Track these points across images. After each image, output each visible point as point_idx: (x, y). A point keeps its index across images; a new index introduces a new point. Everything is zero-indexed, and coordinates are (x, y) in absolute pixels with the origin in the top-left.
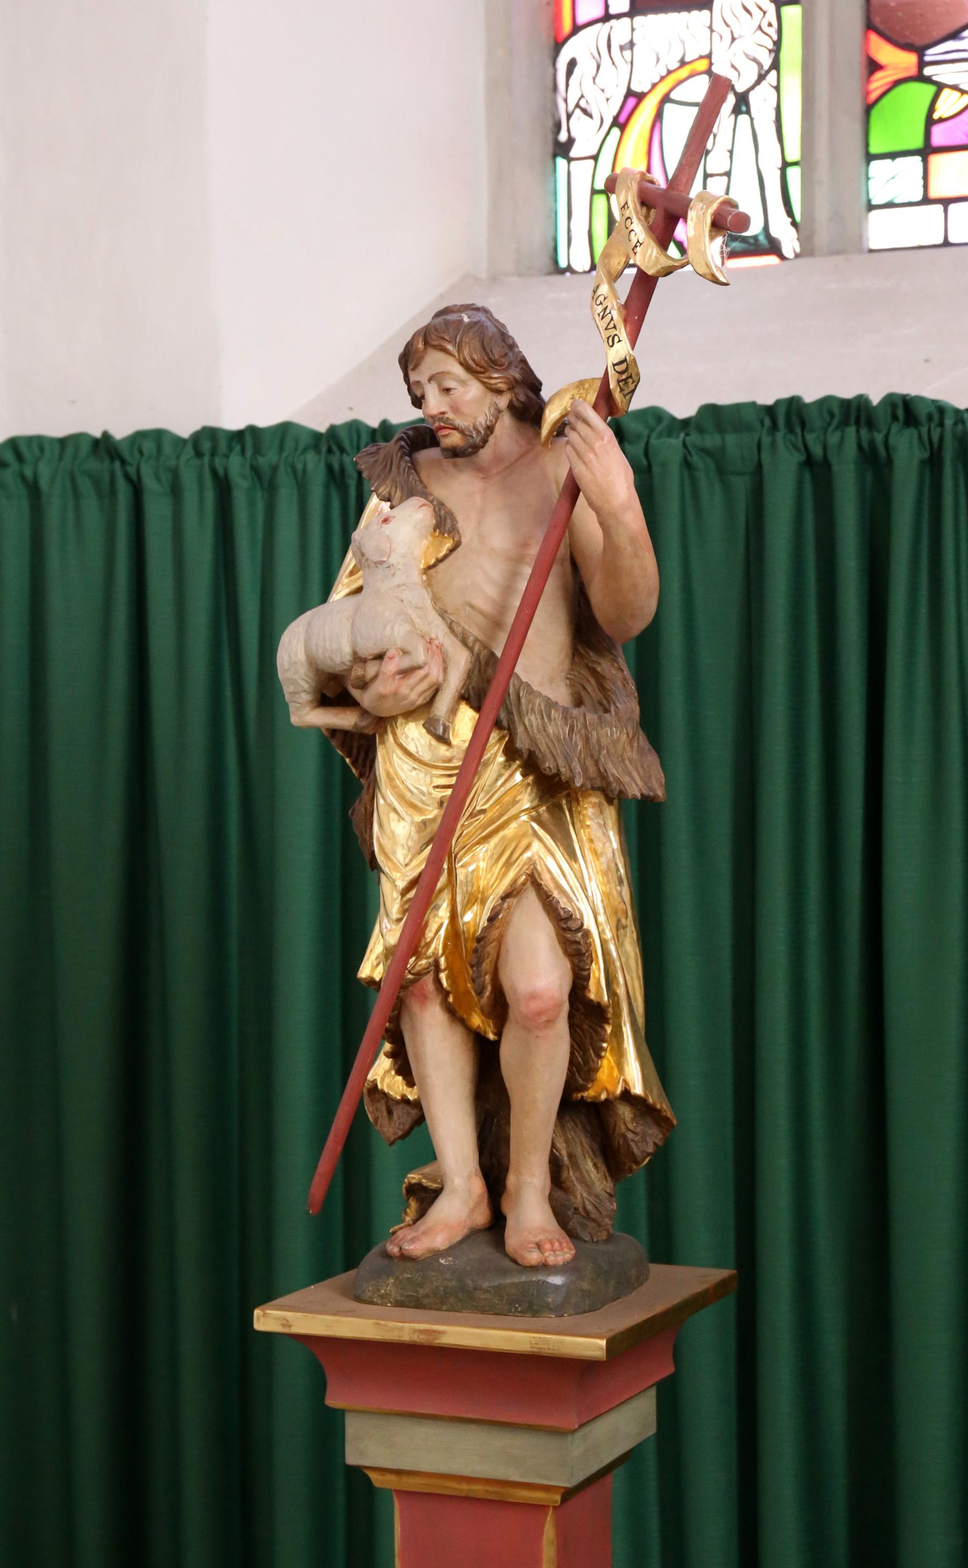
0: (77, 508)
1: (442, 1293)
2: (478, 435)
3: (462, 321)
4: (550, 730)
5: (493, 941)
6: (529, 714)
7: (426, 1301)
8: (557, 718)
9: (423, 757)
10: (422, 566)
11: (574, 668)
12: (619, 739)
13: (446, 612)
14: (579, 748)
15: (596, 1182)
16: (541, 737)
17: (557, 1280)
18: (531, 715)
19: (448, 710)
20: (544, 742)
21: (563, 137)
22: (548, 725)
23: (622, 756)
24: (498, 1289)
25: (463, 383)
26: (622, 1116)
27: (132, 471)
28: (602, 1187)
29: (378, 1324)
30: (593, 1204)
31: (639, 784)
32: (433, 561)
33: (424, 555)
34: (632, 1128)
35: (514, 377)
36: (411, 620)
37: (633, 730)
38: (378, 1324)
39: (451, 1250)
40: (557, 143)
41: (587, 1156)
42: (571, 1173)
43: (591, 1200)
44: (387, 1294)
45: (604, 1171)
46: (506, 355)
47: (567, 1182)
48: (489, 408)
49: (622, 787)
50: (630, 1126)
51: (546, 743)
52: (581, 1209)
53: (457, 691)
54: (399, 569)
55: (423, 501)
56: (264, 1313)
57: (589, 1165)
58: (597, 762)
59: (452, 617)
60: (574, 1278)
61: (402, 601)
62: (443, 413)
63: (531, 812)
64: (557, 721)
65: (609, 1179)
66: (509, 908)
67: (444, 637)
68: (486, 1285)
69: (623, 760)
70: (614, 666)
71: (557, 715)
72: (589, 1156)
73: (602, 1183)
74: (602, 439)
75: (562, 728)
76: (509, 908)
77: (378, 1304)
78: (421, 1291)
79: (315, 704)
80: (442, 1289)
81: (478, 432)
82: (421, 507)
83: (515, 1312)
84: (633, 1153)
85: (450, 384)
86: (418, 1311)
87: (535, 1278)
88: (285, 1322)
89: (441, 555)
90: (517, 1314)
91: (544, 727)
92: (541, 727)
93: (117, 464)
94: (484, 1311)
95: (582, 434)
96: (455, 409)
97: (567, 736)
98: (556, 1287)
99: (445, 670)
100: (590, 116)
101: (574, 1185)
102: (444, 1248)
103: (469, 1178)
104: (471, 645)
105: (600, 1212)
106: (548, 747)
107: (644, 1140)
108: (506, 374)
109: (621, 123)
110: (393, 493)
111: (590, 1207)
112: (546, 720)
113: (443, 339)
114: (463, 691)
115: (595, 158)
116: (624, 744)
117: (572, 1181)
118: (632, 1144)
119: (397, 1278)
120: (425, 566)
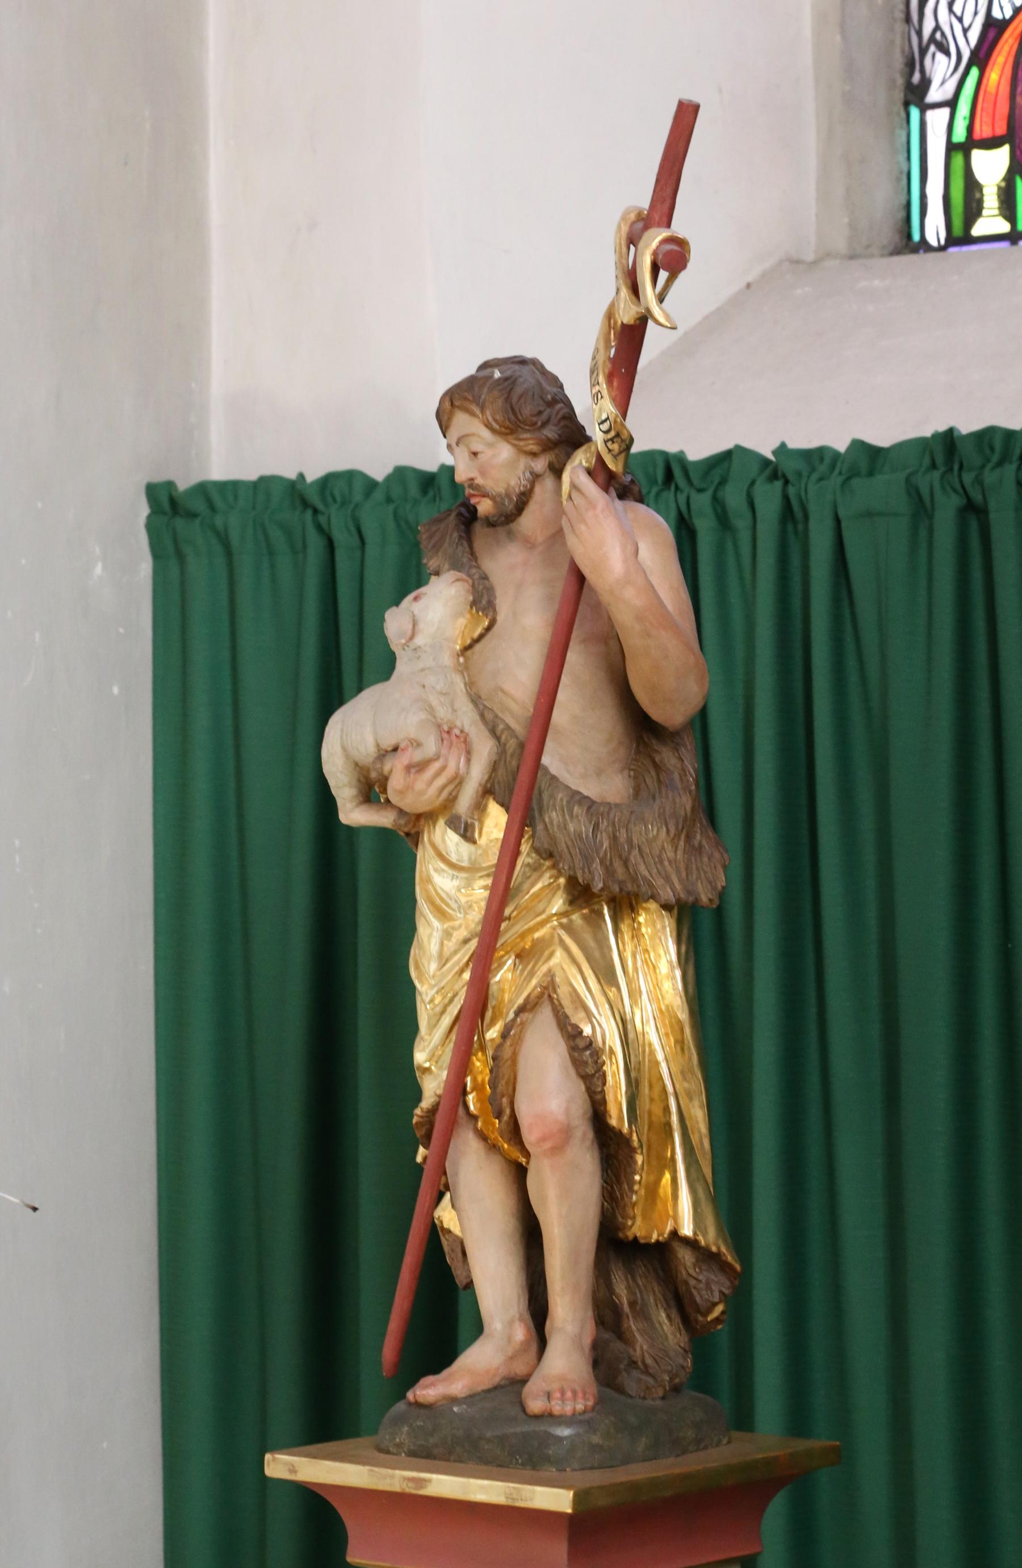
0: (273, 566)
1: (450, 1442)
2: (511, 502)
3: (492, 376)
4: (571, 827)
5: (507, 1060)
6: (550, 810)
7: (436, 1451)
8: (579, 815)
9: (450, 857)
10: (458, 647)
11: (638, 757)
12: (655, 838)
13: (480, 698)
14: (604, 848)
15: (669, 1335)
16: (561, 836)
17: (565, 1432)
18: (552, 811)
19: (470, 806)
20: (563, 841)
21: (916, 78)
22: (569, 821)
23: (660, 856)
24: (502, 1440)
25: (491, 445)
26: (683, 1261)
27: (322, 519)
28: (675, 1341)
29: (372, 1471)
30: (652, 1356)
31: (677, 887)
32: (468, 641)
33: (461, 634)
34: (694, 1274)
35: (546, 436)
36: (431, 706)
37: (677, 828)
38: (372, 1471)
39: (471, 1399)
40: (909, 87)
41: (659, 1306)
42: (632, 1323)
43: (651, 1352)
44: (402, 1443)
45: (678, 1324)
46: (540, 413)
47: (627, 1333)
48: (524, 473)
49: (655, 891)
50: (691, 1271)
51: (566, 842)
52: (640, 1363)
53: (480, 784)
54: (425, 652)
55: (464, 576)
56: (274, 1458)
57: (661, 1316)
58: (626, 863)
59: (486, 703)
60: (581, 1431)
61: (424, 686)
62: (472, 479)
63: (560, 919)
64: (580, 818)
65: (683, 1332)
66: (522, 1023)
67: (470, 726)
68: (489, 1434)
69: (661, 862)
70: (674, 754)
71: (580, 811)
72: (662, 1306)
73: (675, 1336)
74: (594, 507)
75: (585, 827)
76: (522, 1023)
77: (393, 1454)
78: (431, 1440)
79: (361, 799)
80: (449, 1438)
81: (510, 499)
82: (453, 582)
83: (516, 1464)
84: (695, 1301)
85: (476, 447)
86: (430, 1461)
87: (541, 1427)
88: (291, 1468)
89: (476, 635)
90: (518, 1466)
91: (565, 825)
92: (562, 825)
93: (309, 513)
94: (487, 1463)
95: (575, 502)
96: (483, 473)
97: (591, 834)
98: (560, 1439)
99: (468, 761)
100: (947, 53)
101: (634, 1335)
102: (463, 1395)
103: (511, 1323)
104: (498, 733)
105: (659, 1366)
106: (568, 847)
107: (708, 1286)
108: (537, 434)
109: (981, 57)
110: (442, 566)
111: (649, 1361)
112: (567, 817)
113: (466, 399)
114: (489, 785)
115: (952, 104)
116: (663, 842)
117: (632, 1332)
118: (695, 1292)
119: (411, 1426)
120: (462, 648)
